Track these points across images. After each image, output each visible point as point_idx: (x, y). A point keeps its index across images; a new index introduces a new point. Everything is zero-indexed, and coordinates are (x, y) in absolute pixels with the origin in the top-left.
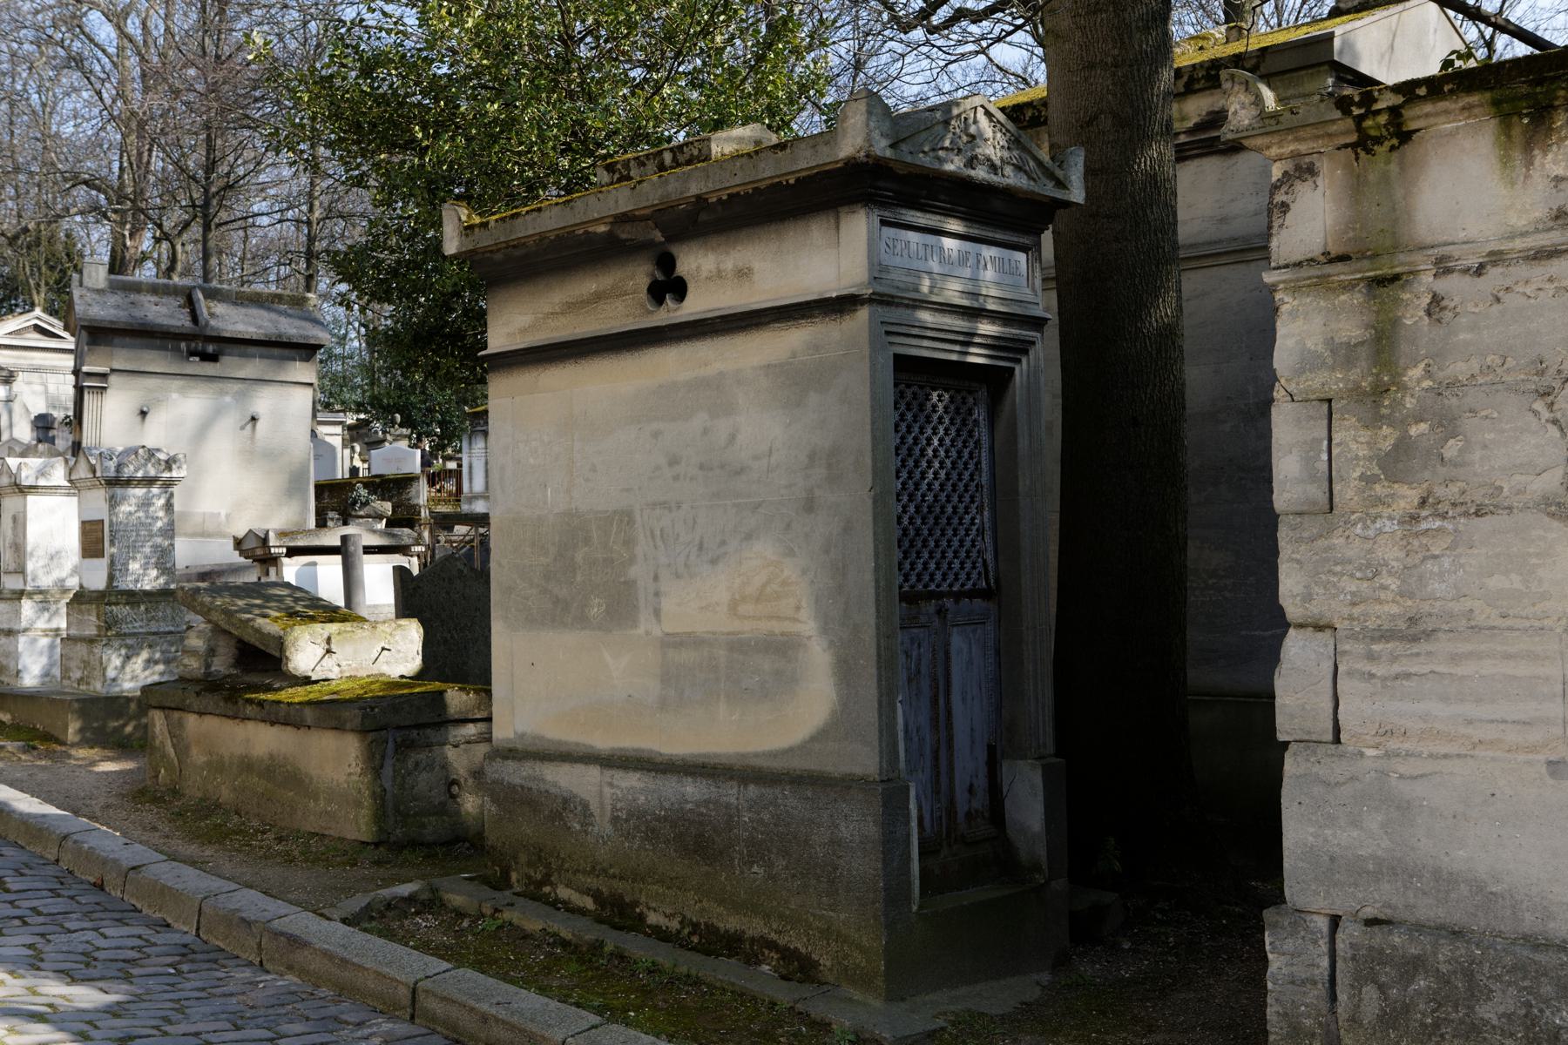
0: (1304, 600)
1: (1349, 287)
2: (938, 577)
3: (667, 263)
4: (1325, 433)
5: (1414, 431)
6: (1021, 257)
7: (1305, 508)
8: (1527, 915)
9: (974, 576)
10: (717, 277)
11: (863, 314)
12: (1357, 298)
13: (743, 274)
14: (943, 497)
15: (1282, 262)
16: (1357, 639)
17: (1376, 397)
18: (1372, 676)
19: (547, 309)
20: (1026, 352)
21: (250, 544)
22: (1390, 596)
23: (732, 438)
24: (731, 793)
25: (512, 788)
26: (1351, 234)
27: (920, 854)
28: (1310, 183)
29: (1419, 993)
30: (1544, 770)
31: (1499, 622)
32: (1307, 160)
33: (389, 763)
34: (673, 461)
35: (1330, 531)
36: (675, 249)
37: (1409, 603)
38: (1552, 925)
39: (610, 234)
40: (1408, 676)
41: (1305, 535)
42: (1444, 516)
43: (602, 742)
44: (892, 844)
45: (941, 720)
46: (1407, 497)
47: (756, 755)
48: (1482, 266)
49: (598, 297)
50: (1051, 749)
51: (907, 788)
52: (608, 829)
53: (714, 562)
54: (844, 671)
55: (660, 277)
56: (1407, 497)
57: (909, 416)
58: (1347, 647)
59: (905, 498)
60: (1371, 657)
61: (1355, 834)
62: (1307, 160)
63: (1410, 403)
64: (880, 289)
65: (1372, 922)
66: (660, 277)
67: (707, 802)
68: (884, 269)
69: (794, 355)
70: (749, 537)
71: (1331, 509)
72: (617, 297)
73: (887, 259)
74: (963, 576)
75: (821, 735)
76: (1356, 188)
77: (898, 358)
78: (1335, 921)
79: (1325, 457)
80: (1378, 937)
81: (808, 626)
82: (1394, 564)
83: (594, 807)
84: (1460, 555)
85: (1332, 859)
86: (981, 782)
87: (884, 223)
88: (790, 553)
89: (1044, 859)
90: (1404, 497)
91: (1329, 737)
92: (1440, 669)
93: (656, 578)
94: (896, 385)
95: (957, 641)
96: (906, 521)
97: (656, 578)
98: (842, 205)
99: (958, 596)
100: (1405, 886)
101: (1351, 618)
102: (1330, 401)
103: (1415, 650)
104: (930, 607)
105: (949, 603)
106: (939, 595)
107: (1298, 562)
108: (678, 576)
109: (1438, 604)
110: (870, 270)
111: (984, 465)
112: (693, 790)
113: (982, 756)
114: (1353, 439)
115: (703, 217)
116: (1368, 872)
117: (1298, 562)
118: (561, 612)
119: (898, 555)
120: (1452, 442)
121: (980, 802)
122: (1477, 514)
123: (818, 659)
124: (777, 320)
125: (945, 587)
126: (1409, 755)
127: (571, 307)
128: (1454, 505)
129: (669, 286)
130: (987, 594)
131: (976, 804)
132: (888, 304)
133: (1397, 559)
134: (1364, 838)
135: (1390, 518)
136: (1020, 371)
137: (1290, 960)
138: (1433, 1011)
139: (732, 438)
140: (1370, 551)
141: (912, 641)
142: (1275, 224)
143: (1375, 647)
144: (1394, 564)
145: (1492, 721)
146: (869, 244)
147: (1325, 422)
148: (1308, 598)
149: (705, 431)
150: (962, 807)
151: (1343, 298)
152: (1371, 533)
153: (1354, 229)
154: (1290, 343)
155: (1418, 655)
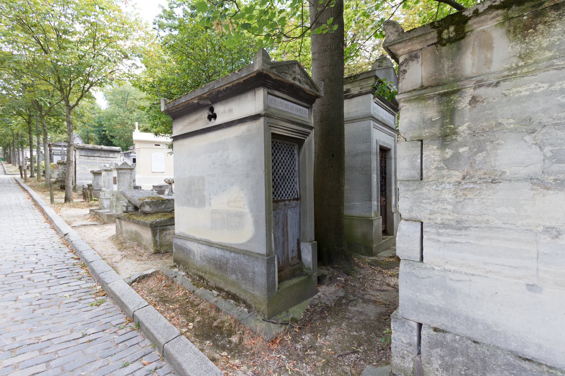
0: (409, 212)
1: (430, 98)
2: (284, 195)
3: (212, 110)
4: (419, 152)
5: (461, 150)
6: (307, 110)
7: (410, 179)
8: (513, 343)
9: (294, 195)
10: (226, 112)
11: (262, 120)
12: (435, 102)
13: (230, 111)
14: (286, 174)
15: (403, 91)
16: (432, 227)
17: (445, 138)
18: (438, 241)
19: (185, 124)
20: (308, 135)
21: (167, 181)
22: (448, 212)
23: (228, 157)
24: (227, 254)
25: (178, 245)
26: (434, 77)
27: (278, 269)
28: (416, 61)
29: (458, 362)
30: (525, 287)
31: (503, 226)
32: (414, 53)
33: (158, 235)
34: (214, 164)
35: (422, 187)
36: (214, 106)
37: (457, 215)
38: (526, 350)
39: (198, 103)
40: (456, 243)
41: (411, 188)
42: (475, 183)
43: (198, 237)
44: (269, 274)
45: (285, 233)
46: (457, 175)
47: (234, 244)
48: (498, 82)
49: (196, 120)
50: (313, 239)
51: (275, 257)
52: (199, 259)
53: (223, 191)
54: (256, 223)
55: (210, 114)
56: (457, 175)
57: (276, 151)
58: (428, 230)
59: (275, 174)
60: (438, 234)
61: (430, 296)
62: (414, 53)
63: (459, 139)
64: (267, 112)
65: (436, 330)
66: (210, 114)
67: (222, 256)
68: (269, 107)
69: (243, 133)
70: (232, 184)
71: (422, 179)
72: (200, 120)
73: (270, 105)
74: (291, 195)
75: (250, 241)
76: (438, 60)
77: (273, 134)
78: (420, 325)
79: (419, 161)
80: (440, 335)
81: (247, 210)
82: (450, 200)
83: (196, 253)
84: (483, 199)
85: (420, 304)
86: (296, 249)
87: (269, 93)
88: (243, 189)
89: (312, 267)
90: (455, 175)
91: (418, 259)
92: (471, 241)
93: (210, 195)
94: (272, 142)
95: (289, 212)
96: (275, 180)
97: (210, 195)
98: (256, 88)
99: (290, 200)
100: (452, 320)
101: (430, 219)
102: (422, 141)
103: (459, 233)
104: (282, 204)
105: (287, 202)
106: (285, 200)
107: (407, 198)
108: (215, 194)
109: (471, 217)
110: (264, 107)
111: (297, 165)
112: (218, 252)
113: (296, 242)
114: (432, 153)
115: (220, 95)
116: (435, 311)
117: (407, 198)
118: (189, 203)
119: (272, 190)
120: (480, 154)
121: (295, 254)
122: (492, 182)
123: (249, 220)
124: (239, 123)
125: (286, 198)
126: (455, 272)
127: (190, 124)
128: (481, 179)
129: (213, 116)
130: (297, 199)
131: (294, 255)
132: (270, 117)
133: (451, 199)
134: (435, 299)
135: (449, 183)
136: (307, 140)
137: (401, 337)
138: (465, 370)
139: (228, 157)
140: (438, 195)
141: (277, 213)
142: (401, 78)
143: (440, 230)
144: (450, 200)
145: (497, 265)
146: (315, 215)
147: (420, 148)
148: (411, 210)
149: (221, 155)
150: (290, 256)
151: (429, 102)
152: (440, 189)
153: (435, 76)
154: (406, 121)
155: (460, 235)
